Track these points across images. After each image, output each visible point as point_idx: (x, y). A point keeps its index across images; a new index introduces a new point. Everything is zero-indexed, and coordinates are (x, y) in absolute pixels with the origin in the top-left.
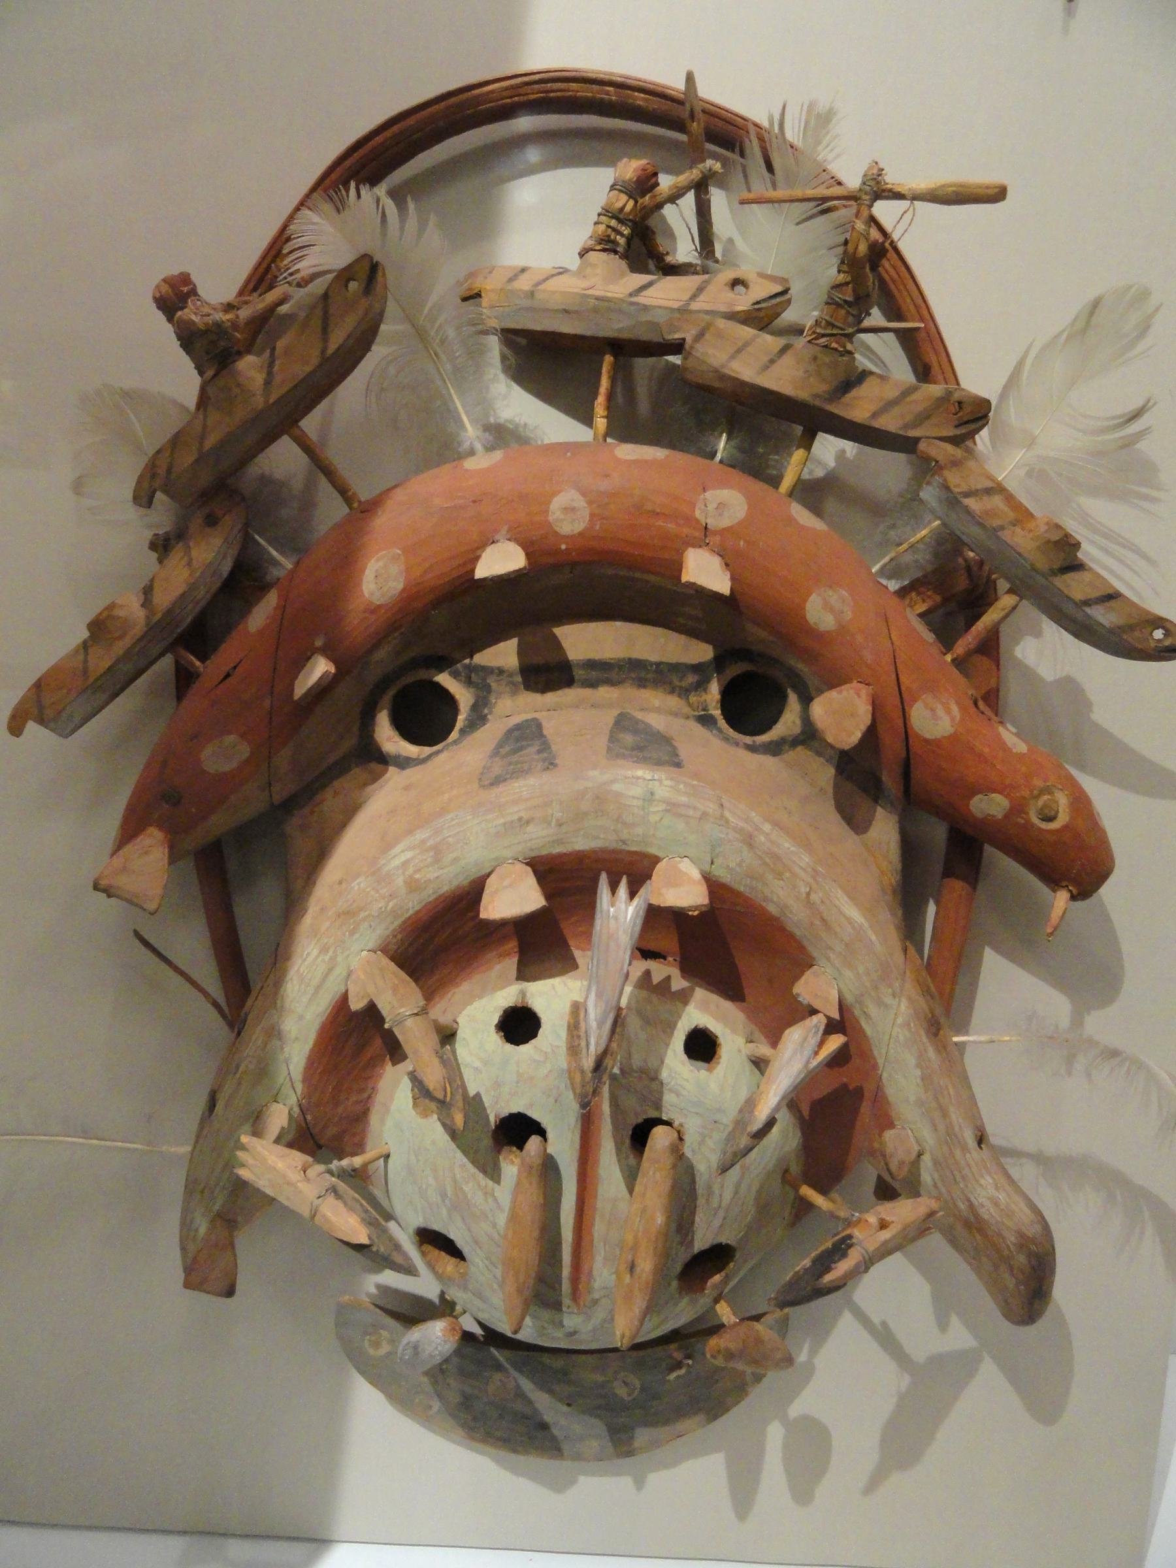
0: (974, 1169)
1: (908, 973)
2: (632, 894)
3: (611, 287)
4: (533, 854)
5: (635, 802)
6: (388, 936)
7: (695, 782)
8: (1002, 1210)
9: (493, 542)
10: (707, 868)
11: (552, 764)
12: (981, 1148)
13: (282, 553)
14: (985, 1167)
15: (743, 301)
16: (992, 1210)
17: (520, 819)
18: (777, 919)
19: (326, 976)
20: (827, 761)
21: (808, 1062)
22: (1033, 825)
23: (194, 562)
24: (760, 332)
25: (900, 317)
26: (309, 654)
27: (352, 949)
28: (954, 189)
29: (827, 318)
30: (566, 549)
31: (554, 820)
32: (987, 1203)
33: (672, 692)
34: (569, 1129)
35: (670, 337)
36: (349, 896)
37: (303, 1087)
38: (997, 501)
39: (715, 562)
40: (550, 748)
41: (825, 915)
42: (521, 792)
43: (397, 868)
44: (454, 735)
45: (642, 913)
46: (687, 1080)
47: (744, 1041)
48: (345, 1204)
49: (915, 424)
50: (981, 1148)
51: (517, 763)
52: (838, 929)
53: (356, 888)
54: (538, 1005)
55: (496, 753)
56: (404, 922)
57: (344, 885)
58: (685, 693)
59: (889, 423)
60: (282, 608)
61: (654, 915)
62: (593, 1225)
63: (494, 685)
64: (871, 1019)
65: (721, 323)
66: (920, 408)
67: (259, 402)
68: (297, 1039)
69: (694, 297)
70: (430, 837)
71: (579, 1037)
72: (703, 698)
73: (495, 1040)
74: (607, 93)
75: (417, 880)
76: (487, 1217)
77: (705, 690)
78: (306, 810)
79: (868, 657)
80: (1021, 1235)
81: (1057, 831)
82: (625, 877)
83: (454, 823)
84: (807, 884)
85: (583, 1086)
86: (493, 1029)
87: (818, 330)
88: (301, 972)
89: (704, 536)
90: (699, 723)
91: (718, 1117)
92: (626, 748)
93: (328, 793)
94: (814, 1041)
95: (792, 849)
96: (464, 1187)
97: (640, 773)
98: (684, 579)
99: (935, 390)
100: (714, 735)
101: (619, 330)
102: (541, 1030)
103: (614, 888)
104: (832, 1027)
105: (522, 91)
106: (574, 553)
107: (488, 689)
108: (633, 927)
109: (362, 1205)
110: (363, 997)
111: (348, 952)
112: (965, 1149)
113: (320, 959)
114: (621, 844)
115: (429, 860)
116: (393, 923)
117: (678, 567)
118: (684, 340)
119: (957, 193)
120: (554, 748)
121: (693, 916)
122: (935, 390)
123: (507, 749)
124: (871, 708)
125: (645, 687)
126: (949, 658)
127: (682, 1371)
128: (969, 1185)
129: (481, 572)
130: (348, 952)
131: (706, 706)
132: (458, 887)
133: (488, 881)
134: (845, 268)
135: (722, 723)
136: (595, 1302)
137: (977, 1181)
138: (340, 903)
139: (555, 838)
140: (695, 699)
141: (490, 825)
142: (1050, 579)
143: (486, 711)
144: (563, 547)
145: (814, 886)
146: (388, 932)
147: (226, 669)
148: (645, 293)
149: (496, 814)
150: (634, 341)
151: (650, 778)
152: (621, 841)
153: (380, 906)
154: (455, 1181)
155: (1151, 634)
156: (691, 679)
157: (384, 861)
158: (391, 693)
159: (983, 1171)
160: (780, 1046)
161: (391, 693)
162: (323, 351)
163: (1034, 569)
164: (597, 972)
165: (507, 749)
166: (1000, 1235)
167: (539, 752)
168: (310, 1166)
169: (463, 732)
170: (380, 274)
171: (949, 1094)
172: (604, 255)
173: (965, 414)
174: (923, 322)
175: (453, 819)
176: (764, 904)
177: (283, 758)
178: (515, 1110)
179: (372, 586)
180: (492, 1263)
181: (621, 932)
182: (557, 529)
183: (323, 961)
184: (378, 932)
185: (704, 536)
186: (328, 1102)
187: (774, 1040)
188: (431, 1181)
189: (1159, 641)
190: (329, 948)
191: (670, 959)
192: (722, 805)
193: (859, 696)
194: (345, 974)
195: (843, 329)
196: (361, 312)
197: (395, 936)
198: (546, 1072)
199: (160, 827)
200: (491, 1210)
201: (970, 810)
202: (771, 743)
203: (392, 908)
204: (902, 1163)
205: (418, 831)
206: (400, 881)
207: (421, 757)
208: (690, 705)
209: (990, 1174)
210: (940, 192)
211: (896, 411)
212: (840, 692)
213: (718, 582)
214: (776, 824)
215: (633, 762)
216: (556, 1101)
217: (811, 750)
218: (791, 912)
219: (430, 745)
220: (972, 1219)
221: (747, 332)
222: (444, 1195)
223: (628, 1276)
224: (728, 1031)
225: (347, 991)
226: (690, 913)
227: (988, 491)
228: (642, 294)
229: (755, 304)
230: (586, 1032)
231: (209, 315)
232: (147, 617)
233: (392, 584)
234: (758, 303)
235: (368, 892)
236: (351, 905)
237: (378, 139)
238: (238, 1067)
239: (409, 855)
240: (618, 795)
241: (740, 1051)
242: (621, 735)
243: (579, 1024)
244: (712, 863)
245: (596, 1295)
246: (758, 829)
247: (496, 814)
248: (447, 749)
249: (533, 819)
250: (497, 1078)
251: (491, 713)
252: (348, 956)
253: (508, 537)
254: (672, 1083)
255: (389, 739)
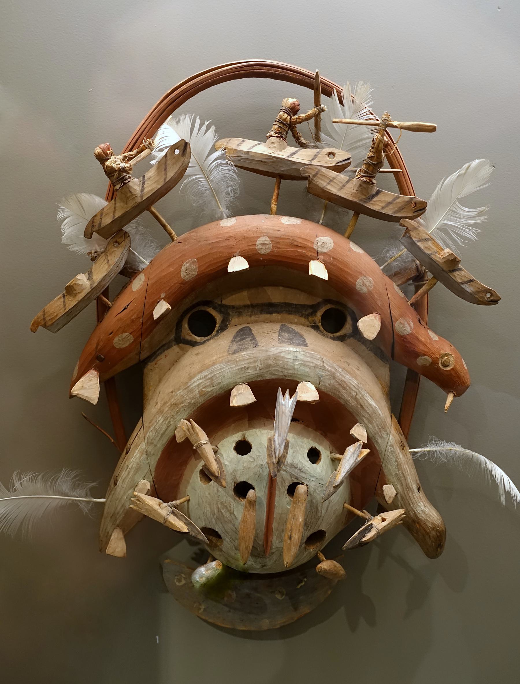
0: (416, 500)
1: (392, 425)
2: (291, 397)
3: (280, 153)
4: (250, 381)
5: (290, 361)
6: (191, 414)
7: (313, 352)
8: (427, 515)
9: (234, 257)
10: (317, 386)
11: (257, 345)
12: (419, 492)
13: (144, 258)
14: (421, 499)
15: (333, 162)
16: (423, 515)
17: (245, 367)
18: (343, 405)
19: (166, 430)
20: (362, 343)
21: (356, 459)
22: (440, 368)
23: (110, 262)
24: (339, 174)
25: (396, 174)
26: (159, 301)
27: (177, 419)
28: (416, 126)
29: (365, 169)
30: (262, 260)
31: (258, 367)
32: (420, 512)
33: (302, 316)
34: (263, 487)
35: (304, 175)
36: (176, 398)
37: (155, 474)
38: (430, 243)
39: (322, 266)
40: (255, 338)
41: (362, 404)
42: (245, 356)
43: (196, 386)
44: (214, 333)
45: (295, 404)
46: (309, 468)
47: (330, 453)
48: (178, 517)
49: (398, 211)
50: (419, 492)
51: (242, 345)
52: (367, 409)
53: (179, 394)
54: (250, 439)
55: (233, 341)
56: (198, 408)
57: (173, 393)
58: (307, 316)
59: (389, 211)
60: (147, 281)
61: (300, 405)
62: (272, 523)
63: (230, 313)
64: (378, 443)
65: (324, 170)
66: (400, 205)
67: (139, 200)
68: (153, 454)
69: (313, 159)
70: (209, 374)
71: (272, 451)
72: (314, 319)
73: (234, 453)
74: (278, 71)
75: (204, 391)
76: (231, 522)
77: (315, 315)
78: (154, 363)
79: (379, 303)
80: (433, 524)
81: (449, 371)
82: (288, 389)
83: (218, 369)
84: (355, 392)
85: (274, 469)
86: (233, 449)
87: (362, 174)
88: (156, 427)
89: (316, 255)
90: (312, 328)
91: (321, 482)
92: (285, 338)
93: (162, 356)
94: (357, 452)
95: (350, 378)
96: (222, 511)
97: (291, 349)
98: (310, 273)
99: (406, 197)
100: (319, 333)
101: (283, 171)
102: (252, 449)
103: (284, 395)
104: (364, 446)
105: (243, 69)
106: (265, 262)
107: (228, 314)
108: (292, 409)
109: (185, 518)
110: (182, 437)
111: (175, 420)
112: (413, 492)
113: (164, 423)
114: (284, 376)
115: (209, 383)
116: (194, 408)
117: (307, 268)
118: (309, 176)
119: (418, 128)
120: (257, 339)
121: (313, 404)
122: (406, 197)
123: (238, 339)
124: (380, 324)
125: (291, 314)
126: (409, 303)
127: (303, 584)
128: (415, 506)
129: (230, 269)
130: (175, 420)
131: (315, 322)
132: (219, 394)
133: (232, 391)
134: (373, 150)
135: (321, 328)
136: (273, 553)
137: (417, 504)
138: (172, 400)
139: (258, 374)
140: (311, 319)
141: (233, 370)
142: (449, 274)
143: (227, 323)
144: (261, 259)
145: (358, 392)
146: (191, 412)
147: (125, 305)
148: (294, 156)
149: (235, 365)
150: (288, 175)
151: (295, 351)
152: (284, 375)
153: (189, 401)
154: (218, 508)
155: (486, 295)
156: (310, 311)
157: (190, 384)
158: (189, 315)
159: (420, 500)
160: (345, 454)
161: (189, 315)
162: (165, 179)
163: (443, 270)
164: (278, 426)
165: (238, 339)
166: (425, 524)
167: (251, 340)
168: (162, 504)
169: (218, 331)
170: (188, 147)
171: (407, 471)
172: (277, 139)
173: (417, 208)
174: (401, 169)
175: (218, 367)
176: (339, 400)
177: (146, 342)
178: (242, 480)
179: (185, 274)
180: (233, 539)
181: (287, 411)
182: (259, 252)
183: (165, 423)
184: (188, 412)
185: (316, 255)
186: (230, 458)
187: (342, 453)
188: (208, 509)
189: (489, 298)
190: (168, 418)
191: (301, 421)
192: (323, 361)
193: (376, 319)
194: (174, 428)
195: (372, 174)
196: (180, 164)
197: (194, 414)
198: (254, 465)
199: (96, 370)
200: (233, 519)
201: (417, 363)
202: (340, 336)
203: (194, 402)
204: (390, 497)
205: (204, 372)
206: (197, 392)
207: (201, 341)
208: (309, 321)
209: (422, 502)
210: (412, 127)
211: (391, 206)
212: (369, 317)
213: (323, 274)
214: (344, 369)
215: (289, 344)
216: (258, 476)
217: (355, 339)
218: (349, 403)
219: (205, 337)
220: (415, 518)
221: (334, 174)
222: (214, 514)
223: (289, 540)
224: (323, 449)
225: (175, 435)
226: (312, 403)
227: (426, 240)
228: (293, 157)
229: (337, 163)
230: (274, 449)
231: (119, 164)
232: (91, 285)
233: (193, 273)
234: (339, 163)
235: (184, 396)
236: (177, 401)
237: (184, 87)
238: (128, 466)
239: (200, 381)
240: (283, 357)
241: (328, 456)
242: (283, 334)
243: (272, 445)
244: (319, 384)
245: (273, 551)
246: (336, 370)
247: (235, 365)
248: (212, 338)
249: (250, 367)
250: (235, 468)
251: (229, 324)
252: (176, 421)
253: (239, 255)
254: (303, 469)
255: (188, 334)
